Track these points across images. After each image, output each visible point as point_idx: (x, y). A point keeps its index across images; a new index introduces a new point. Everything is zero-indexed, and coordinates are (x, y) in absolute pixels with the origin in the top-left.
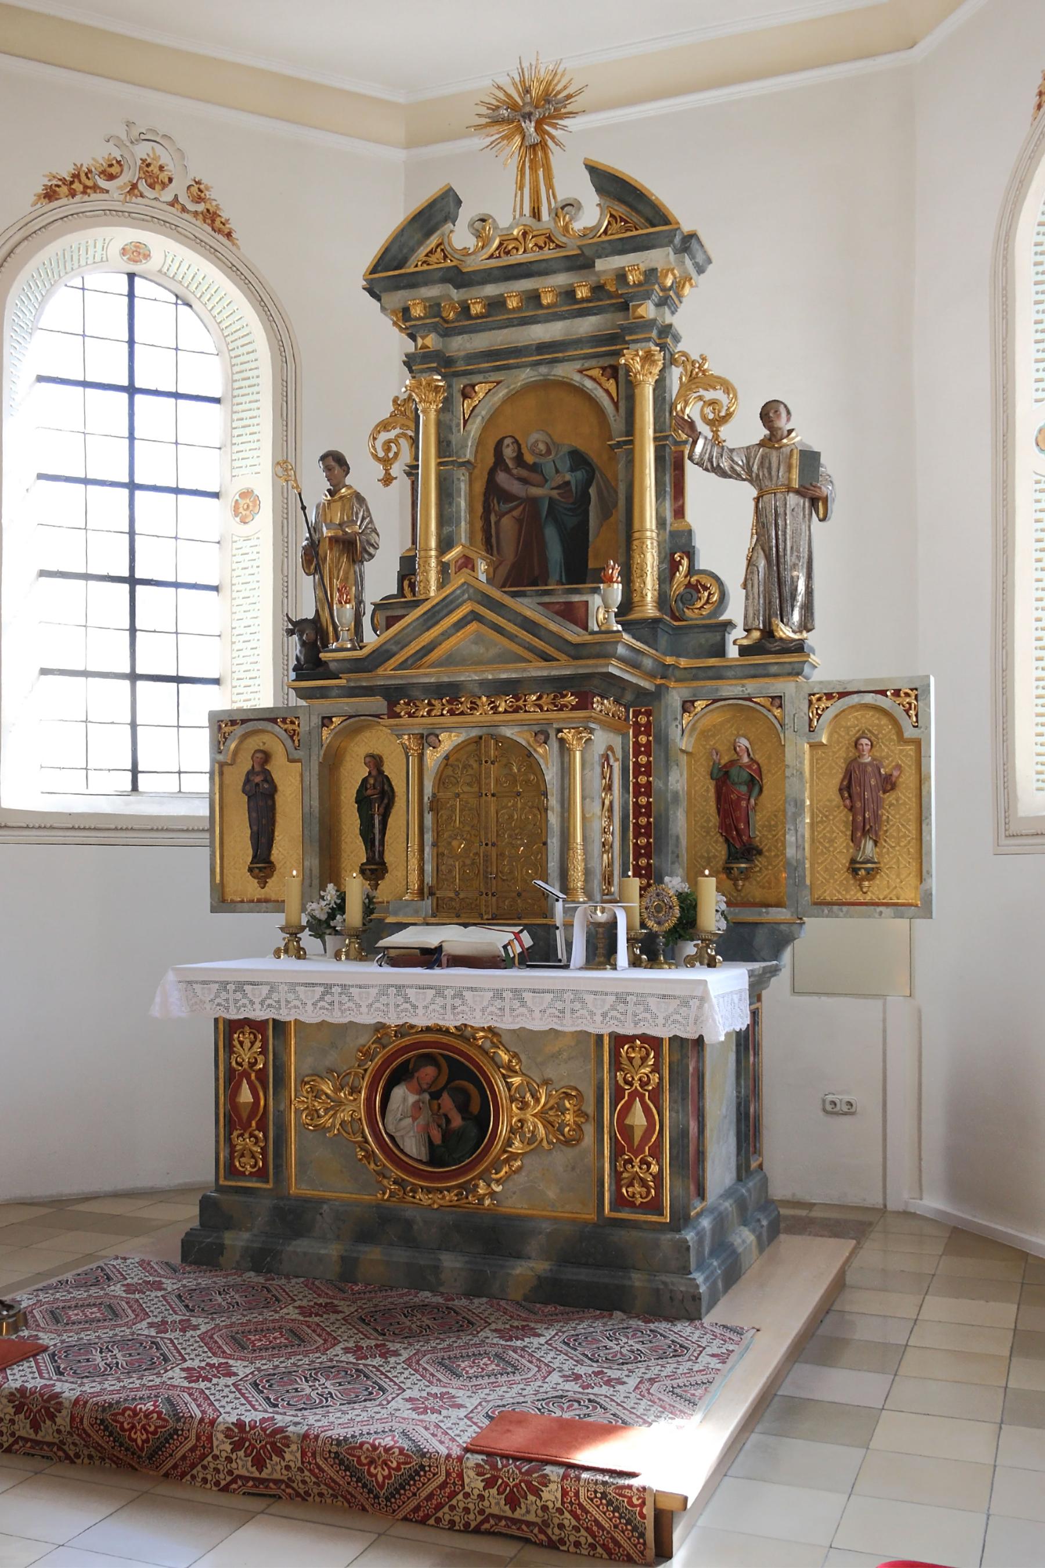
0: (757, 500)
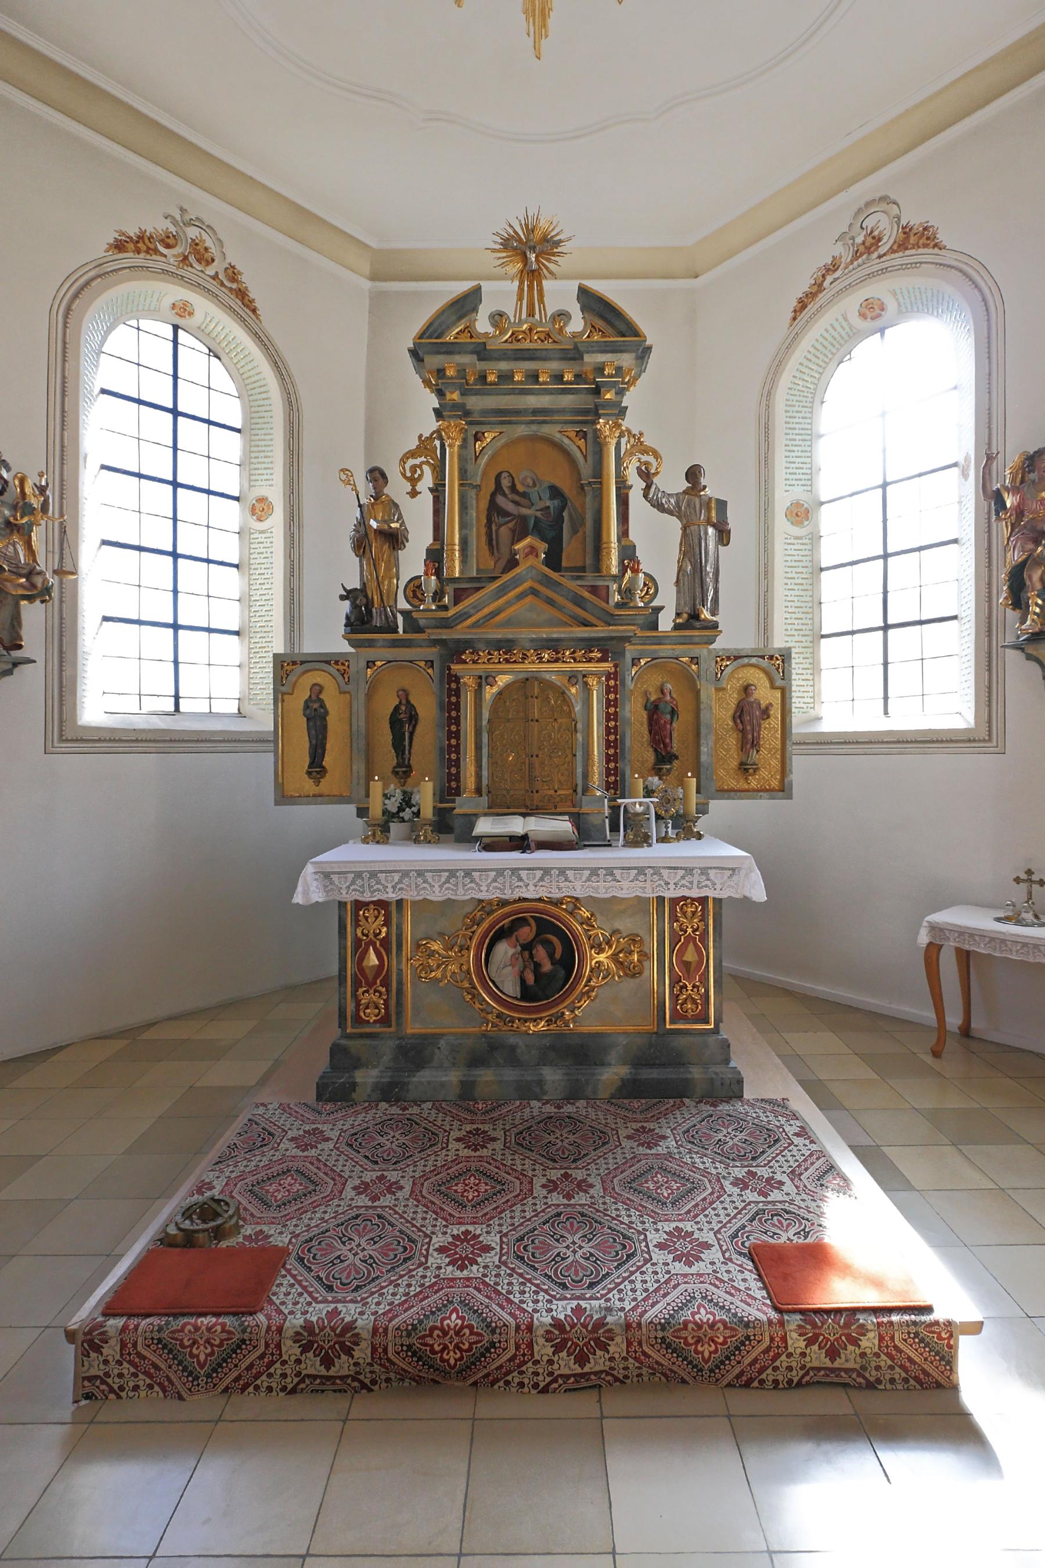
0: (684, 529)
